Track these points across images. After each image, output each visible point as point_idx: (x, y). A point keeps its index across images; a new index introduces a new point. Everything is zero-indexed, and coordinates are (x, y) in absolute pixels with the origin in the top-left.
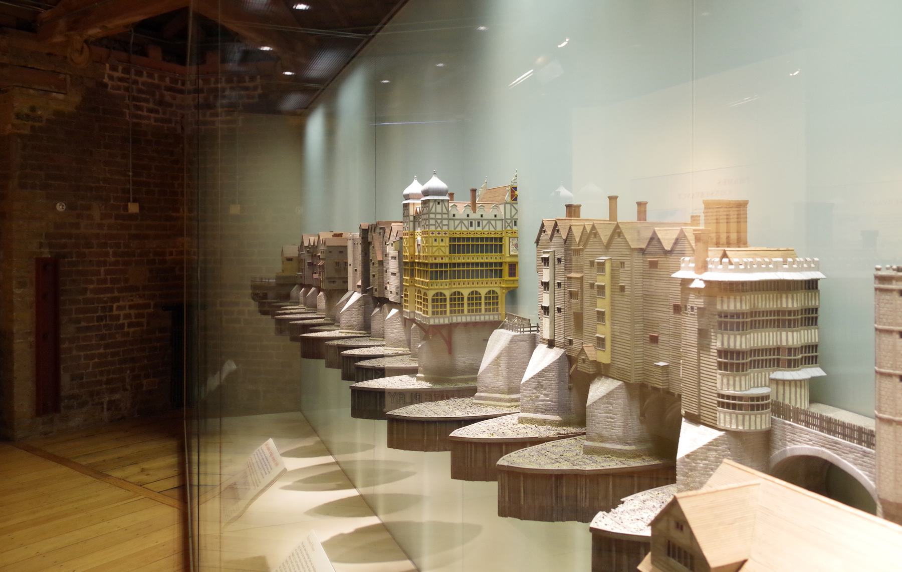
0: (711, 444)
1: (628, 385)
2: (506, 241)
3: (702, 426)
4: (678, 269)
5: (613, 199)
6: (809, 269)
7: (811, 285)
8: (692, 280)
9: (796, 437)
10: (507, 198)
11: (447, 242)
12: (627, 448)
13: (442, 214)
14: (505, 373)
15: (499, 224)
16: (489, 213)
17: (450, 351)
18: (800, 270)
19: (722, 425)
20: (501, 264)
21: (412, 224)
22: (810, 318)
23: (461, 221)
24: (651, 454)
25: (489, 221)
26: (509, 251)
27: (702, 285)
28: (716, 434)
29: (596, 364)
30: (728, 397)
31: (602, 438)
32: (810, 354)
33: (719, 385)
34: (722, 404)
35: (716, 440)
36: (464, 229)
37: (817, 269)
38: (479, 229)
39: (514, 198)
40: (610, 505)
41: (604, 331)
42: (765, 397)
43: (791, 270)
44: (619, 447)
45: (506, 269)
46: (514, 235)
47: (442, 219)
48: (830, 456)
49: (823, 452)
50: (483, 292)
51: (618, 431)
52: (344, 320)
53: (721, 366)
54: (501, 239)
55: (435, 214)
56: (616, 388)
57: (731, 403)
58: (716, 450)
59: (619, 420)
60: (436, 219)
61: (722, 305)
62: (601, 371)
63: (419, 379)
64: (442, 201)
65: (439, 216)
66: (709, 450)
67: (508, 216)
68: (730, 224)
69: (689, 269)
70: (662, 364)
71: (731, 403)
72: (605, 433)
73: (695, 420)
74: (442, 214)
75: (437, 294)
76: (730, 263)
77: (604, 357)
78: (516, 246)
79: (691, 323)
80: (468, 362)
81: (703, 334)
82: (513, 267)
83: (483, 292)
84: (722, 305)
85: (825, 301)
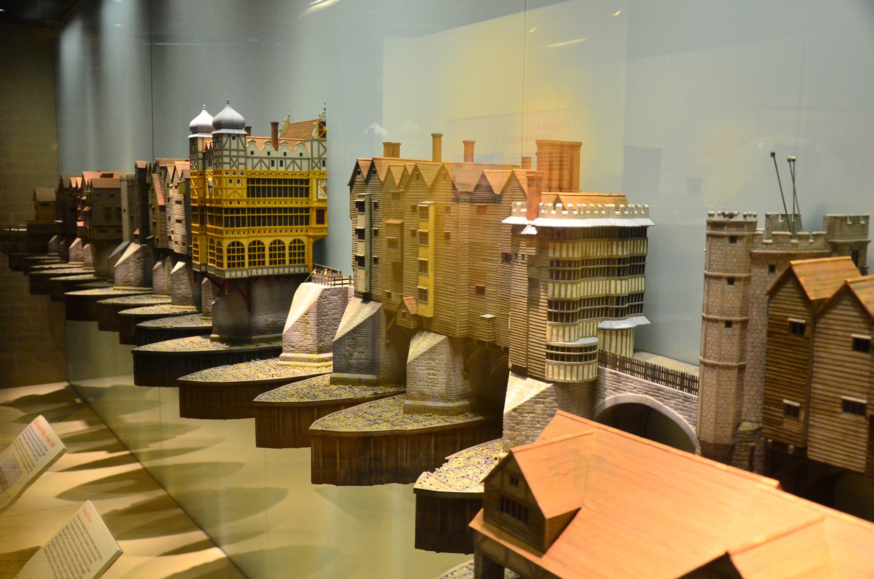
0: (538, 396)
1: (448, 337)
2: (313, 184)
3: (529, 379)
4: (510, 214)
5: (437, 137)
6: (640, 216)
7: (640, 233)
8: (523, 227)
9: (622, 386)
10: (315, 134)
11: (244, 184)
12: (450, 405)
13: (238, 150)
14: (314, 331)
15: (305, 164)
16: (293, 151)
17: (250, 307)
18: (632, 216)
19: (549, 377)
20: (307, 210)
21: (201, 162)
22: (635, 266)
23: (261, 159)
24: (472, 410)
25: (294, 160)
26: (317, 194)
27: (534, 232)
28: (544, 386)
29: (418, 318)
30: (557, 348)
31: (423, 396)
32: (633, 304)
33: (548, 337)
34: (550, 356)
35: (543, 392)
36: (264, 169)
37: (647, 216)
38: (282, 169)
39: (323, 135)
40: (434, 464)
41: (427, 282)
42: (593, 347)
43: (623, 216)
44: (441, 404)
45: (313, 215)
46: (323, 177)
47: (238, 157)
48: (653, 402)
49: (647, 399)
50: (287, 241)
51: (440, 388)
52: (119, 275)
53: (550, 316)
54: (307, 181)
55: (230, 150)
56: (440, 343)
57: (559, 354)
58: (543, 403)
59: (441, 377)
60: (230, 157)
61: (554, 253)
62: (423, 325)
63: (213, 340)
64: (238, 135)
65: (234, 153)
66: (536, 403)
67: (315, 155)
68: (560, 167)
69: (520, 214)
70: (488, 316)
71: (559, 354)
72: (427, 391)
73: (522, 373)
74: (238, 150)
75: (233, 244)
76: (564, 209)
77: (427, 310)
78: (325, 189)
79: (520, 272)
80: (270, 320)
81: (533, 284)
82: (321, 215)
83: (287, 241)
84: (554, 253)
85: (655, 250)
